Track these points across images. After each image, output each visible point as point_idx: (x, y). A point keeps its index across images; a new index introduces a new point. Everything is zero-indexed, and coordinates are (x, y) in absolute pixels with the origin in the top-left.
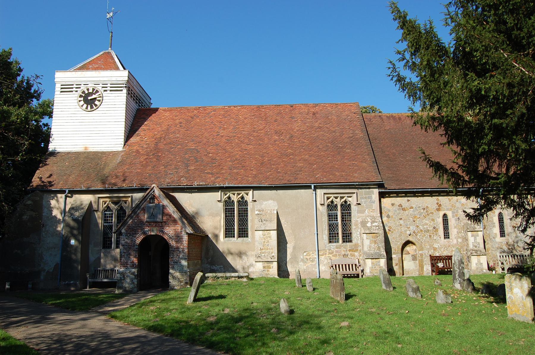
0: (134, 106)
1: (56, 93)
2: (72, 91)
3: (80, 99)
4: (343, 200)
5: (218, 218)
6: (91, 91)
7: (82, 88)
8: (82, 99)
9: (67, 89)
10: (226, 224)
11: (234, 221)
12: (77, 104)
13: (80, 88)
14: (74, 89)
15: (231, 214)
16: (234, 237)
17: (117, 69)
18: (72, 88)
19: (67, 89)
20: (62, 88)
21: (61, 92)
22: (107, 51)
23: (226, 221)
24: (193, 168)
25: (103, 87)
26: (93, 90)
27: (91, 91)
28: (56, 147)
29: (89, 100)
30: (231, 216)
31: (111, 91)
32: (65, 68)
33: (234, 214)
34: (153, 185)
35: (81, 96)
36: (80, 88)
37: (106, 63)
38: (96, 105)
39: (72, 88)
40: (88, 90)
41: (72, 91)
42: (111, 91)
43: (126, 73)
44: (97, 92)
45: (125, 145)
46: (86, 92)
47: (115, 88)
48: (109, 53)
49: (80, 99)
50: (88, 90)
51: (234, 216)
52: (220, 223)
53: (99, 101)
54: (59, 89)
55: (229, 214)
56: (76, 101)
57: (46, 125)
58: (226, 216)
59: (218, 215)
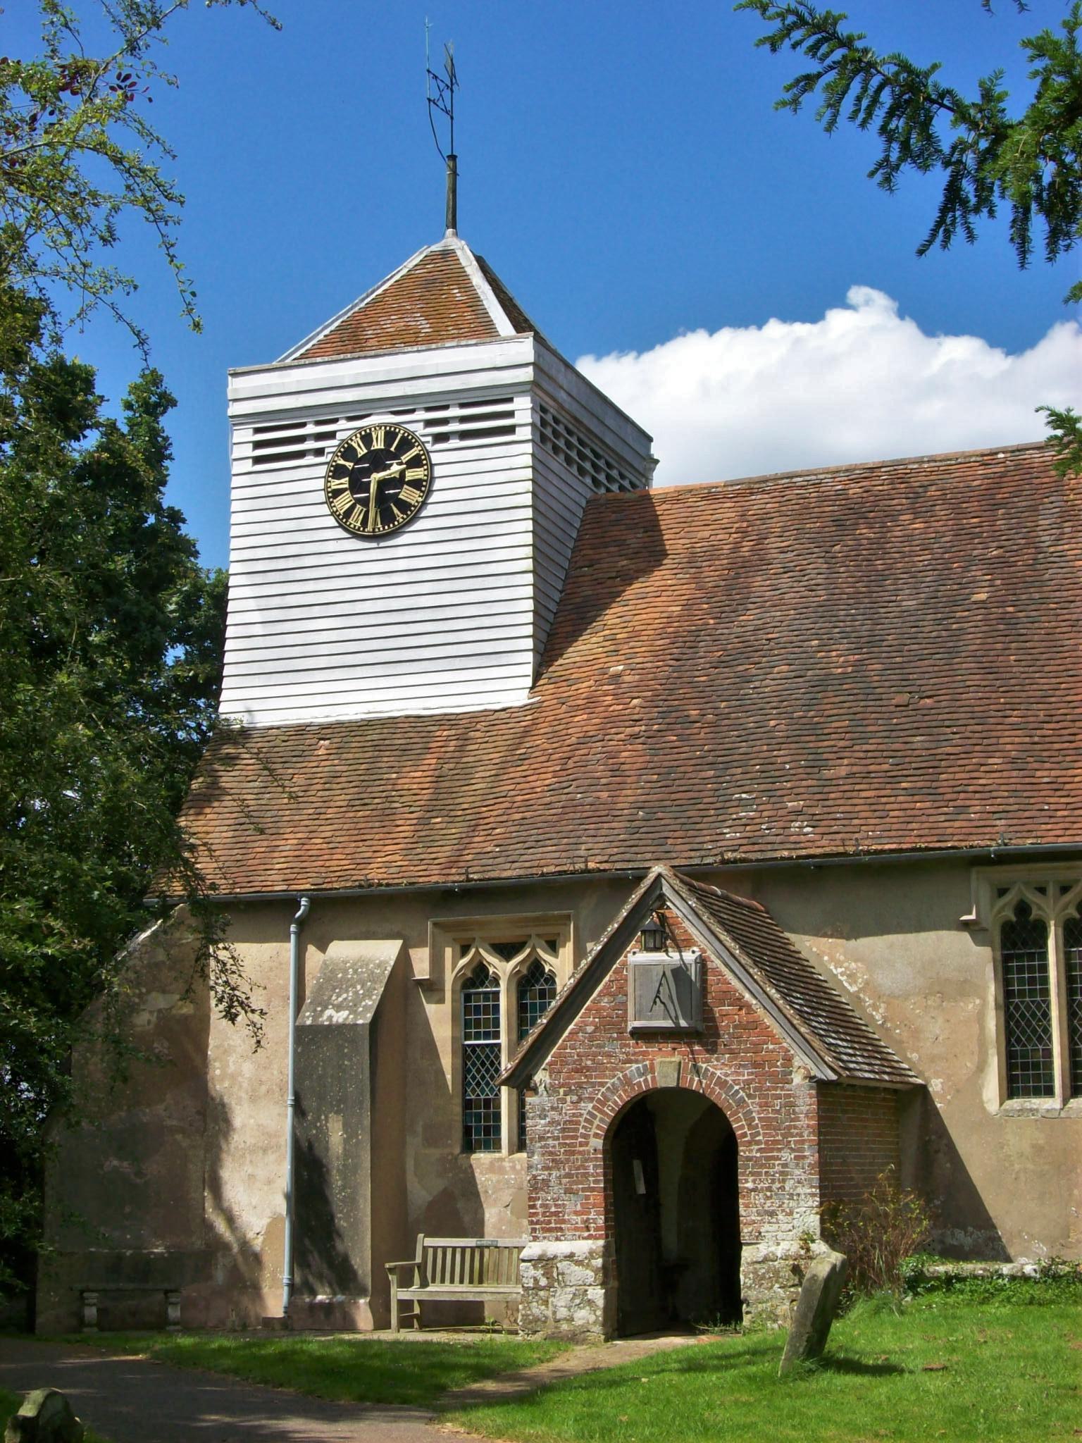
0: (577, 491)
1: (237, 468)
2: (301, 454)
3: (335, 484)
4: (1011, 897)
5: (972, 1005)
6: (379, 445)
7: (339, 436)
8: (344, 482)
9: (280, 438)
10: (1009, 1033)
11: (1046, 1015)
12: (325, 509)
13: (332, 435)
14: (310, 445)
15: (1032, 981)
16: (1049, 1092)
17: (486, 331)
18: (301, 439)
19: (280, 438)
20: (258, 445)
21: (258, 460)
22: (436, 247)
23: (1009, 1017)
24: (843, 771)
25: (429, 423)
26: (390, 436)
27: (379, 445)
28: (254, 705)
29: (379, 489)
30: (1032, 993)
31: (464, 435)
32: (264, 356)
33: (1045, 980)
34: (657, 869)
35: (338, 472)
36: (332, 435)
37: (437, 310)
38: (404, 506)
39: (301, 439)
40: (367, 439)
41: (301, 454)
42: (464, 435)
43: (524, 349)
44: (407, 444)
45: (537, 676)
46: (362, 451)
47: (479, 416)
48: (447, 254)
49: (335, 484)
50: (367, 439)
51: (1045, 992)
52: (982, 1028)
53: (416, 484)
54: (248, 451)
55: (1021, 981)
56: (321, 497)
57: (850, 1297)
58: (1008, 994)
59: (965, 988)
